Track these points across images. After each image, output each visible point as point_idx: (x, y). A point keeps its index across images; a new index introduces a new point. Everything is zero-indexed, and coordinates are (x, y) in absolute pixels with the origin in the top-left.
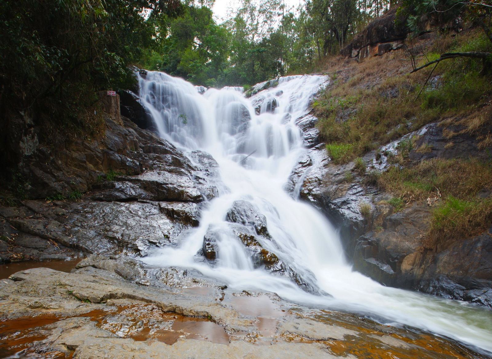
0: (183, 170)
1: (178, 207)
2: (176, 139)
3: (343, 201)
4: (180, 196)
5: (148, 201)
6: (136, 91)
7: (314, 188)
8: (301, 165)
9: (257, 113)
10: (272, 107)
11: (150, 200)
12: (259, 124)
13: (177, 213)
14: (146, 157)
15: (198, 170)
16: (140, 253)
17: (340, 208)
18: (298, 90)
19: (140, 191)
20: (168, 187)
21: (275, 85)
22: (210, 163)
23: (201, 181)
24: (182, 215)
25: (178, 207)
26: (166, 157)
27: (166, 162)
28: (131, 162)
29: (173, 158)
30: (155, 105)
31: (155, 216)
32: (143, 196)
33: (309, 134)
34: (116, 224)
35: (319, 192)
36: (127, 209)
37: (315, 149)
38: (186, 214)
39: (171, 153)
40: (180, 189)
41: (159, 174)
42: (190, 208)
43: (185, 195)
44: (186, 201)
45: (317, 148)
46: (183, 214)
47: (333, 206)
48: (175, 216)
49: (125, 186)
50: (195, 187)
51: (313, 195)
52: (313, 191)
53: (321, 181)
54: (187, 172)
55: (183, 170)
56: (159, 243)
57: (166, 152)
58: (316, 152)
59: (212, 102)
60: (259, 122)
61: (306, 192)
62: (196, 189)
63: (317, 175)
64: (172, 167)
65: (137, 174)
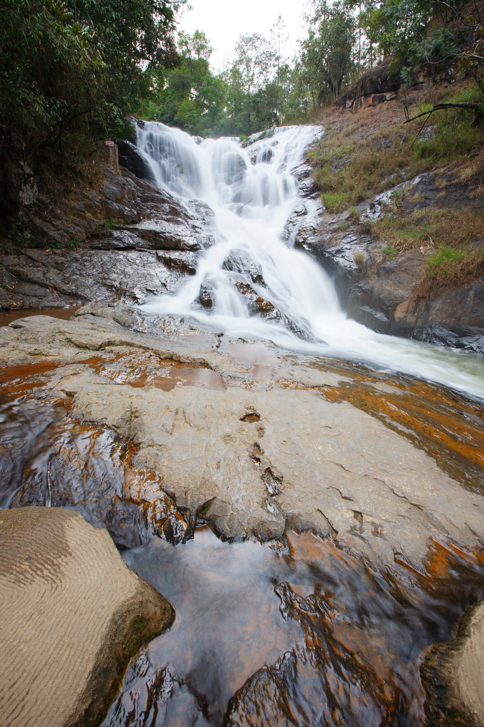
0: (180, 219)
1: (175, 255)
2: (173, 188)
4: (176, 245)
8: (296, 214)
11: (148, 249)
12: (255, 173)
13: (174, 261)
17: (334, 256)
18: (293, 141)
21: (270, 136)
25: (175, 255)
27: (164, 211)
29: (170, 207)
30: (152, 155)
35: (313, 241)
36: (125, 257)
39: (168, 203)
40: (177, 238)
41: (156, 223)
44: (183, 250)
45: (312, 198)
47: (327, 255)
48: (172, 264)
50: (192, 236)
51: (308, 244)
54: (184, 221)
55: (180, 219)
57: (163, 201)
58: (311, 201)
60: (255, 172)
61: (301, 240)
62: (193, 238)
63: (312, 224)
64: (169, 216)
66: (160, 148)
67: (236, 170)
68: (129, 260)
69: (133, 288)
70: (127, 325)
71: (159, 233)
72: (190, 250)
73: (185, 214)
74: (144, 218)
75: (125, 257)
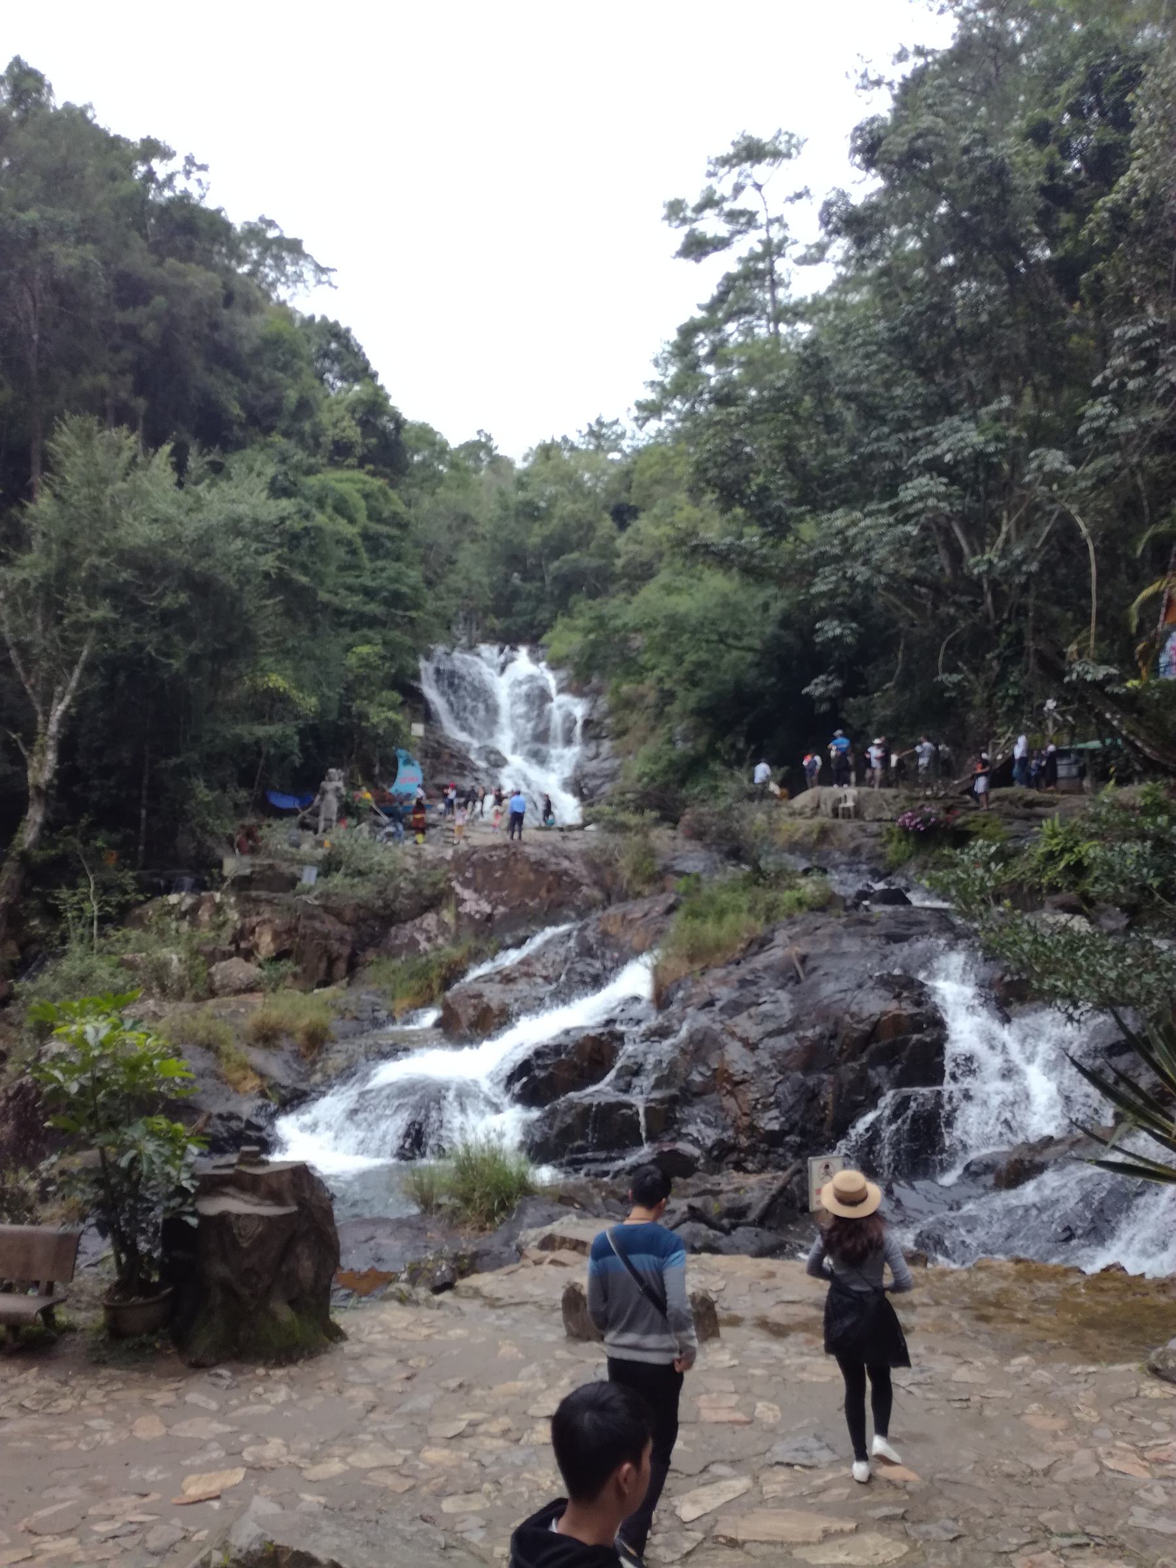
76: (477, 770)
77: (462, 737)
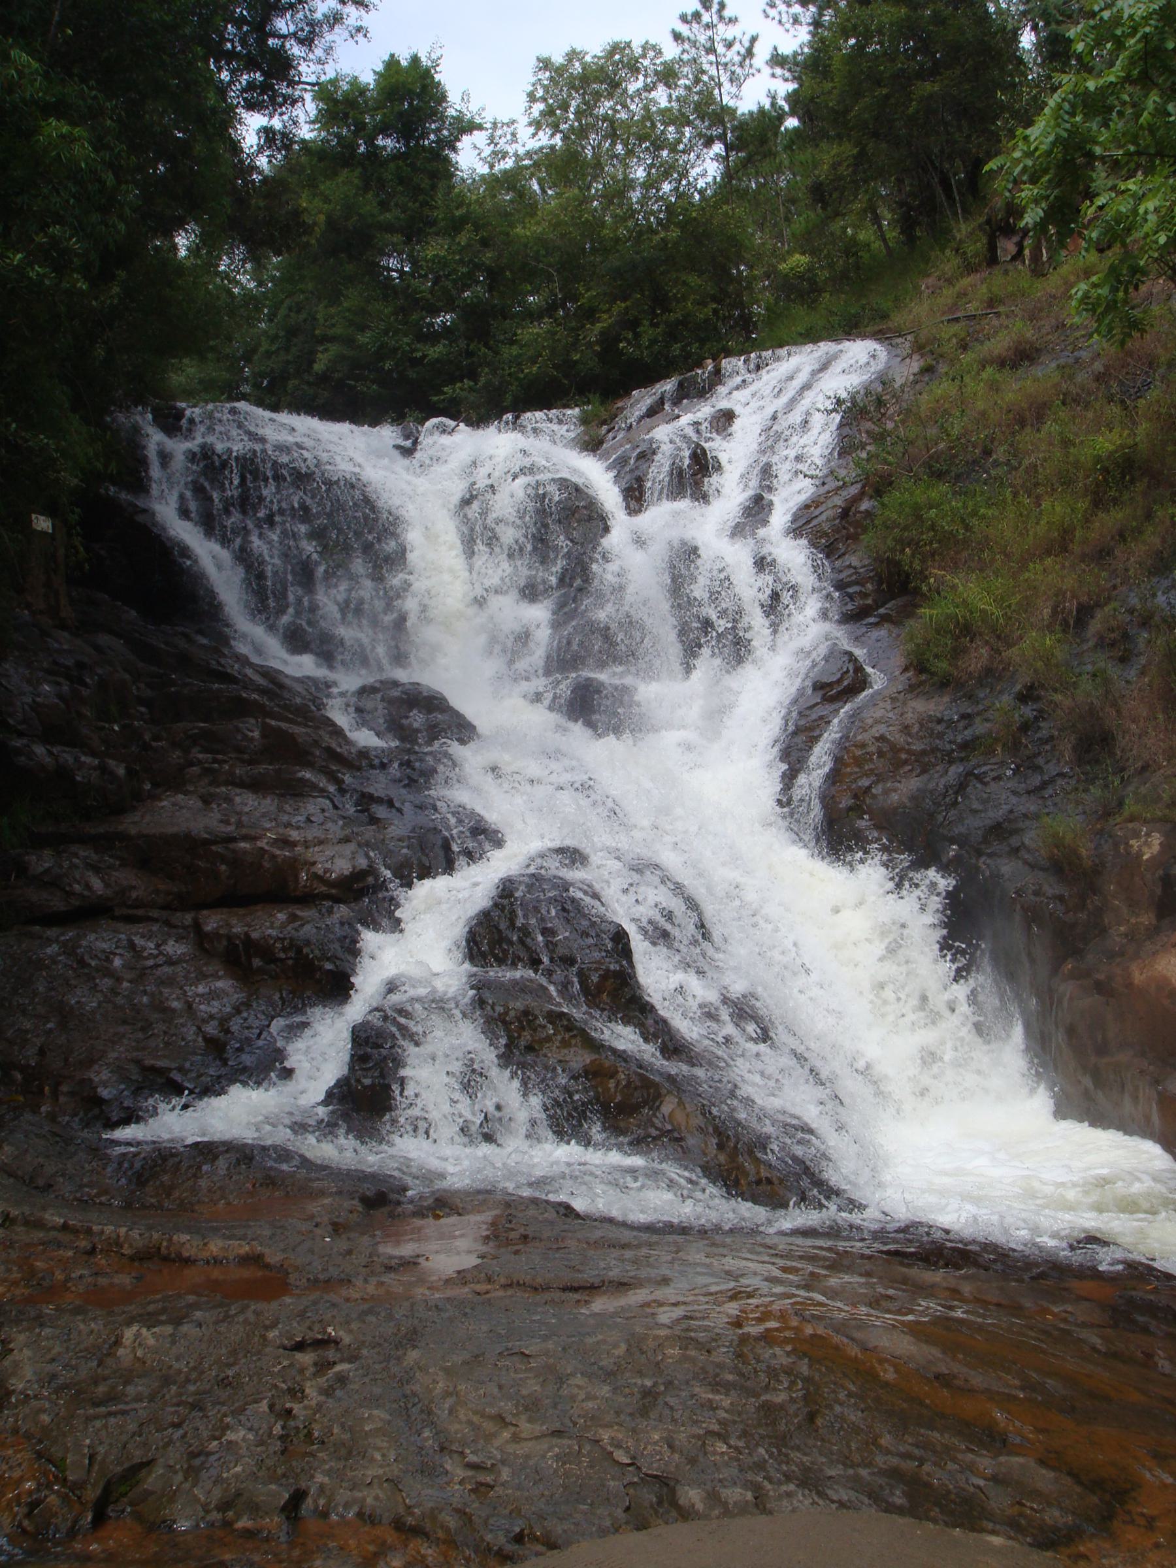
1: (270, 924)
2: (296, 641)
3: (988, 822)
4: (281, 886)
5: (155, 913)
6: (140, 485)
7: (876, 782)
9: (633, 504)
10: (695, 474)
11: (166, 907)
12: (634, 547)
13: (263, 949)
14: (156, 738)
15: (373, 767)
16: (102, 1111)
17: (979, 853)
18: (787, 408)
19: (126, 877)
20: (234, 851)
21: (704, 392)
22: (435, 726)
23: (381, 812)
24: (282, 955)
26: (238, 730)
27: (239, 750)
28: (95, 769)
29: (267, 732)
30: (209, 524)
31: (179, 969)
32: (134, 895)
33: (850, 566)
34: (24, 1012)
35: (895, 797)
36: (70, 950)
37: (876, 624)
38: (299, 951)
39: (260, 711)
41: (207, 800)
42: (313, 926)
43: (304, 876)
44: (307, 899)
45: (885, 619)
46: (284, 949)
48: (257, 962)
49: (66, 864)
50: (346, 840)
52: (874, 797)
53: (902, 749)
54: (323, 782)
56: (180, 1069)
57: (242, 708)
59: (447, 486)
60: (639, 541)
62: (351, 847)
64: (263, 768)
65: (120, 810)
66: (237, 490)
67: (564, 529)
68: (82, 963)
69: (90, 1062)
70: (41, 1182)
71: (206, 842)
72: (338, 900)
73: (330, 751)
74: (155, 785)
75: (70, 950)
76: (363, 760)
77: (303, 666)
